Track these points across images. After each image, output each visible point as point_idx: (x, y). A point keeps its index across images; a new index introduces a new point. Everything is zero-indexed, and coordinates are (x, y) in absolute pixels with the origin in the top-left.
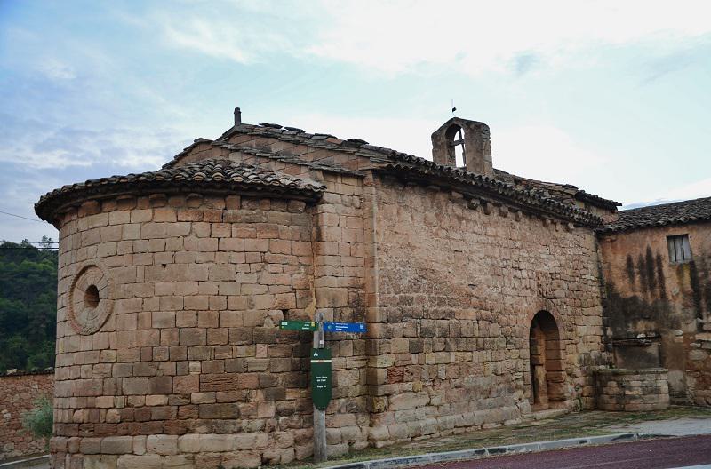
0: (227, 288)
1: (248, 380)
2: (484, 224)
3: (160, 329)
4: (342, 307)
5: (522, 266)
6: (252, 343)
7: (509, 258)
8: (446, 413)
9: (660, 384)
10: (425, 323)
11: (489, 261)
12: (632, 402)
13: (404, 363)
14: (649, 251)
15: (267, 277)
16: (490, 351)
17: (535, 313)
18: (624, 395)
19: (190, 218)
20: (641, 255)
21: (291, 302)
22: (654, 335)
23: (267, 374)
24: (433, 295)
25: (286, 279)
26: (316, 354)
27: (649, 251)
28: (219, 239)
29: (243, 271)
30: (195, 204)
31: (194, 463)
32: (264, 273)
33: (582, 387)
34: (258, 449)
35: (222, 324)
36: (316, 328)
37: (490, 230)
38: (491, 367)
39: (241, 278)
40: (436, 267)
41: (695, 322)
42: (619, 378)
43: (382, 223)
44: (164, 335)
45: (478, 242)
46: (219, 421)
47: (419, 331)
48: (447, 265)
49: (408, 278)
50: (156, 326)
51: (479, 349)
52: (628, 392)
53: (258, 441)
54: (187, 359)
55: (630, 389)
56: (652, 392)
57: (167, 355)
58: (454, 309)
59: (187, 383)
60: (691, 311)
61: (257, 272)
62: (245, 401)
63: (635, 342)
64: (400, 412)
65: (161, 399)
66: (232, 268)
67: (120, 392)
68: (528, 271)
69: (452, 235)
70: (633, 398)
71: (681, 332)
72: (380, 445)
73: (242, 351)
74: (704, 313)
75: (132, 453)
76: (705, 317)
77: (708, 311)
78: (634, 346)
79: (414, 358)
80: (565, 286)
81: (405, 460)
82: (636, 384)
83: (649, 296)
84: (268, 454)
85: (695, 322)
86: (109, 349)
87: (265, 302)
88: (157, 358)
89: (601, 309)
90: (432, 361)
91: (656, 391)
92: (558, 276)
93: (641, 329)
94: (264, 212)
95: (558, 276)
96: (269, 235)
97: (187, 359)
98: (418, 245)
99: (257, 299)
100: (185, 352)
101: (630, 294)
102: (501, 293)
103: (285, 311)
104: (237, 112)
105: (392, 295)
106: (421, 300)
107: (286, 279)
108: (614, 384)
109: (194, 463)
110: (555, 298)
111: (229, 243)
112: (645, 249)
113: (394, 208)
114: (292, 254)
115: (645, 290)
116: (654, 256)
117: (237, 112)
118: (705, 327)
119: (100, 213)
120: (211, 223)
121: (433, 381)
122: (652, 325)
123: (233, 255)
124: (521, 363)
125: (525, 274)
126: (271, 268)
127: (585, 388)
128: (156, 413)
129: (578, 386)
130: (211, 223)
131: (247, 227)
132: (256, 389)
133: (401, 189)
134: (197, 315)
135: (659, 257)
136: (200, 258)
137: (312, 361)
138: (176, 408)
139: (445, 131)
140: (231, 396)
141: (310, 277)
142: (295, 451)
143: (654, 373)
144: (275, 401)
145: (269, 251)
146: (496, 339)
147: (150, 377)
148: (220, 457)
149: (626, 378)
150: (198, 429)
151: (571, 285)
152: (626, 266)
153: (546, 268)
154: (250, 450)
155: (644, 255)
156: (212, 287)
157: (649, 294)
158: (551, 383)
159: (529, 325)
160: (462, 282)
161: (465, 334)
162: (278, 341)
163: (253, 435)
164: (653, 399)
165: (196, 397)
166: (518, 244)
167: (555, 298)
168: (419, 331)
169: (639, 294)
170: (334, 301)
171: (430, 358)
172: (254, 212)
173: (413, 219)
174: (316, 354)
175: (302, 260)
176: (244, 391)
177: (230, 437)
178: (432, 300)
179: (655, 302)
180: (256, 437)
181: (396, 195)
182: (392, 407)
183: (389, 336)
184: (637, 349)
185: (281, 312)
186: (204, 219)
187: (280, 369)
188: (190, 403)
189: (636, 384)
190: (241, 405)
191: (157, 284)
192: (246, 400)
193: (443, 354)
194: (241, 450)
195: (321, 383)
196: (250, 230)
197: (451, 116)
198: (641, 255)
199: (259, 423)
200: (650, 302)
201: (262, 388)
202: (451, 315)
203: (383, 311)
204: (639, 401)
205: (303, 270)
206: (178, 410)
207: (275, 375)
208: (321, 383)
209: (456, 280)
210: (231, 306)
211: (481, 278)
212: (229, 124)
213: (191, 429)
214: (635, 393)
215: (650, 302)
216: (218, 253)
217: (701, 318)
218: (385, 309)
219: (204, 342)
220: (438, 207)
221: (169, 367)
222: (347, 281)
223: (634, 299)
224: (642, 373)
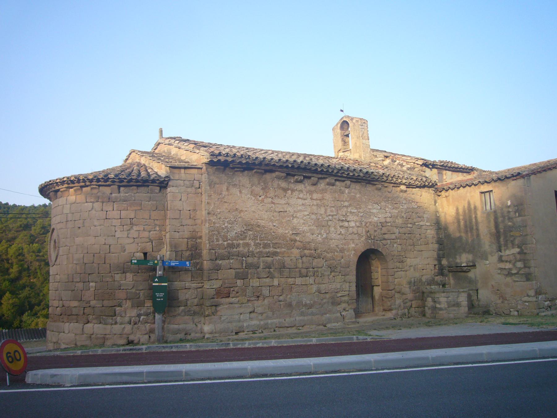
0: (111, 241)
1: (121, 295)
2: (311, 192)
3: (76, 264)
4: (182, 250)
5: (350, 218)
6: (124, 273)
7: (335, 213)
8: (268, 318)
9: (461, 300)
10: (250, 260)
11: (313, 217)
12: (441, 312)
13: (231, 286)
14: (469, 204)
15: (133, 233)
16: (313, 278)
17: (363, 251)
18: (436, 307)
19: (92, 200)
20: (464, 206)
21: (149, 248)
22: (471, 264)
23: (134, 290)
24: (258, 241)
25: (146, 234)
26: (156, 280)
27: (469, 204)
28: (107, 211)
29: (119, 231)
30: (276, 158)
31: (91, 340)
32: (132, 231)
33: (412, 301)
34: (126, 334)
35: (107, 261)
36: (157, 264)
37: (315, 196)
38: (314, 288)
39: (118, 234)
40: (262, 223)
41: (497, 255)
42: (433, 295)
43: (212, 197)
44: (78, 267)
45: (303, 204)
46: (104, 317)
47: (244, 265)
48: (272, 221)
49: (235, 231)
50: (75, 262)
51: (301, 276)
52: (438, 306)
53: (126, 330)
54: (89, 281)
55: (440, 303)
56: (454, 305)
57: (79, 279)
58: (278, 250)
59: (88, 295)
60: (495, 247)
61: (128, 230)
62: (119, 306)
63: (460, 269)
64: (225, 317)
65: (75, 304)
66: (113, 228)
67: (60, 300)
68: (356, 222)
69: (276, 201)
70: (441, 309)
71: (488, 262)
72: (207, 336)
73: (117, 277)
74: (503, 248)
75: (64, 332)
76: (503, 251)
77: (505, 247)
78: (460, 272)
79: (239, 282)
80: (397, 231)
81: (170, 346)
82: (443, 300)
83: (470, 236)
84: (131, 338)
85: (497, 255)
86: (57, 274)
87: (131, 248)
88: (75, 280)
89: (436, 246)
90: (258, 284)
91: (458, 305)
92: (389, 224)
93: (464, 259)
94: (133, 194)
95: (389, 224)
96: (136, 208)
97: (89, 281)
98: (244, 209)
99: (127, 247)
100: (87, 277)
101: (458, 235)
102: (326, 238)
103: (145, 254)
104: (161, 131)
105: (220, 242)
106: (248, 245)
107: (146, 234)
108: (429, 299)
109: (91, 340)
110: (385, 239)
111: (111, 214)
112: (466, 202)
113: (224, 187)
114: (150, 219)
115: (466, 232)
116: (472, 207)
117: (161, 131)
118: (504, 259)
119: (56, 199)
120: (103, 202)
121: (258, 297)
122: (470, 257)
123: (114, 221)
124: (346, 286)
125: (352, 224)
126: (135, 228)
127: (413, 302)
128: (75, 311)
129: (407, 301)
130: (103, 202)
131: (123, 204)
132: (126, 299)
133: (241, 175)
134: (94, 256)
135: (475, 208)
136: (96, 223)
137: (154, 284)
138: (83, 308)
139: (339, 125)
140: (111, 303)
141: (163, 232)
142: (150, 337)
143: (456, 292)
144: (138, 307)
145: (135, 217)
146: (320, 269)
147: (72, 291)
148: (104, 338)
149: (437, 295)
150: (94, 321)
151: (401, 230)
152: (455, 215)
153: (376, 219)
154: (121, 335)
155: (466, 206)
156: (102, 240)
157: (469, 234)
158: (384, 298)
159: (356, 259)
160: (287, 232)
161: (288, 266)
162: (140, 271)
163: (123, 326)
164: (455, 310)
165: (93, 303)
166: (346, 204)
167: (385, 239)
168: (244, 265)
169: (463, 235)
170: (175, 247)
171: (255, 282)
172: (127, 195)
173: (240, 192)
174: (156, 280)
175: (157, 222)
176: (119, 300)
177: (109, 327)
178: (257, 245)
179: (473, 240)
180: (124, 328)
181: (226, 177)
182: (219, 313)
183: (218, 268)
184: (462, 274)
185: (142, 255)
186: (99, 200)
187: (141, 288)
188: (90, 306)
189: (443, 300)
190: (118, 309)
191: (76, 239)
192: (120, 305)
193: (267, 280)
194: (115, 334)
195: (159, 298)
196: (125, 205)
197: (342, 115)
198: (464, 206)
199: (127, 319)
200: (470, 241)
201: (129, 299)
202: (275, 254)
203: (212, 253)
204: (444, 312)
205: (157, 228)
206: (84, 310)
207: (138, 292)
208: (159, 298)
209: (281, 231)
210: (112, 250)
211: (306, 228)
212: (156, 138)
213: (90, 320)
214: (442, 306)
215: (470, 241)
216: (106, 220)
217: (500, 251)
218: (213, 251)
219: (97, 272)
220: (265, 184)
221: (80, 285)
222: (187, 234)
223: (460, 238)
224: (447, 292)
